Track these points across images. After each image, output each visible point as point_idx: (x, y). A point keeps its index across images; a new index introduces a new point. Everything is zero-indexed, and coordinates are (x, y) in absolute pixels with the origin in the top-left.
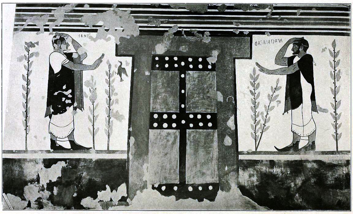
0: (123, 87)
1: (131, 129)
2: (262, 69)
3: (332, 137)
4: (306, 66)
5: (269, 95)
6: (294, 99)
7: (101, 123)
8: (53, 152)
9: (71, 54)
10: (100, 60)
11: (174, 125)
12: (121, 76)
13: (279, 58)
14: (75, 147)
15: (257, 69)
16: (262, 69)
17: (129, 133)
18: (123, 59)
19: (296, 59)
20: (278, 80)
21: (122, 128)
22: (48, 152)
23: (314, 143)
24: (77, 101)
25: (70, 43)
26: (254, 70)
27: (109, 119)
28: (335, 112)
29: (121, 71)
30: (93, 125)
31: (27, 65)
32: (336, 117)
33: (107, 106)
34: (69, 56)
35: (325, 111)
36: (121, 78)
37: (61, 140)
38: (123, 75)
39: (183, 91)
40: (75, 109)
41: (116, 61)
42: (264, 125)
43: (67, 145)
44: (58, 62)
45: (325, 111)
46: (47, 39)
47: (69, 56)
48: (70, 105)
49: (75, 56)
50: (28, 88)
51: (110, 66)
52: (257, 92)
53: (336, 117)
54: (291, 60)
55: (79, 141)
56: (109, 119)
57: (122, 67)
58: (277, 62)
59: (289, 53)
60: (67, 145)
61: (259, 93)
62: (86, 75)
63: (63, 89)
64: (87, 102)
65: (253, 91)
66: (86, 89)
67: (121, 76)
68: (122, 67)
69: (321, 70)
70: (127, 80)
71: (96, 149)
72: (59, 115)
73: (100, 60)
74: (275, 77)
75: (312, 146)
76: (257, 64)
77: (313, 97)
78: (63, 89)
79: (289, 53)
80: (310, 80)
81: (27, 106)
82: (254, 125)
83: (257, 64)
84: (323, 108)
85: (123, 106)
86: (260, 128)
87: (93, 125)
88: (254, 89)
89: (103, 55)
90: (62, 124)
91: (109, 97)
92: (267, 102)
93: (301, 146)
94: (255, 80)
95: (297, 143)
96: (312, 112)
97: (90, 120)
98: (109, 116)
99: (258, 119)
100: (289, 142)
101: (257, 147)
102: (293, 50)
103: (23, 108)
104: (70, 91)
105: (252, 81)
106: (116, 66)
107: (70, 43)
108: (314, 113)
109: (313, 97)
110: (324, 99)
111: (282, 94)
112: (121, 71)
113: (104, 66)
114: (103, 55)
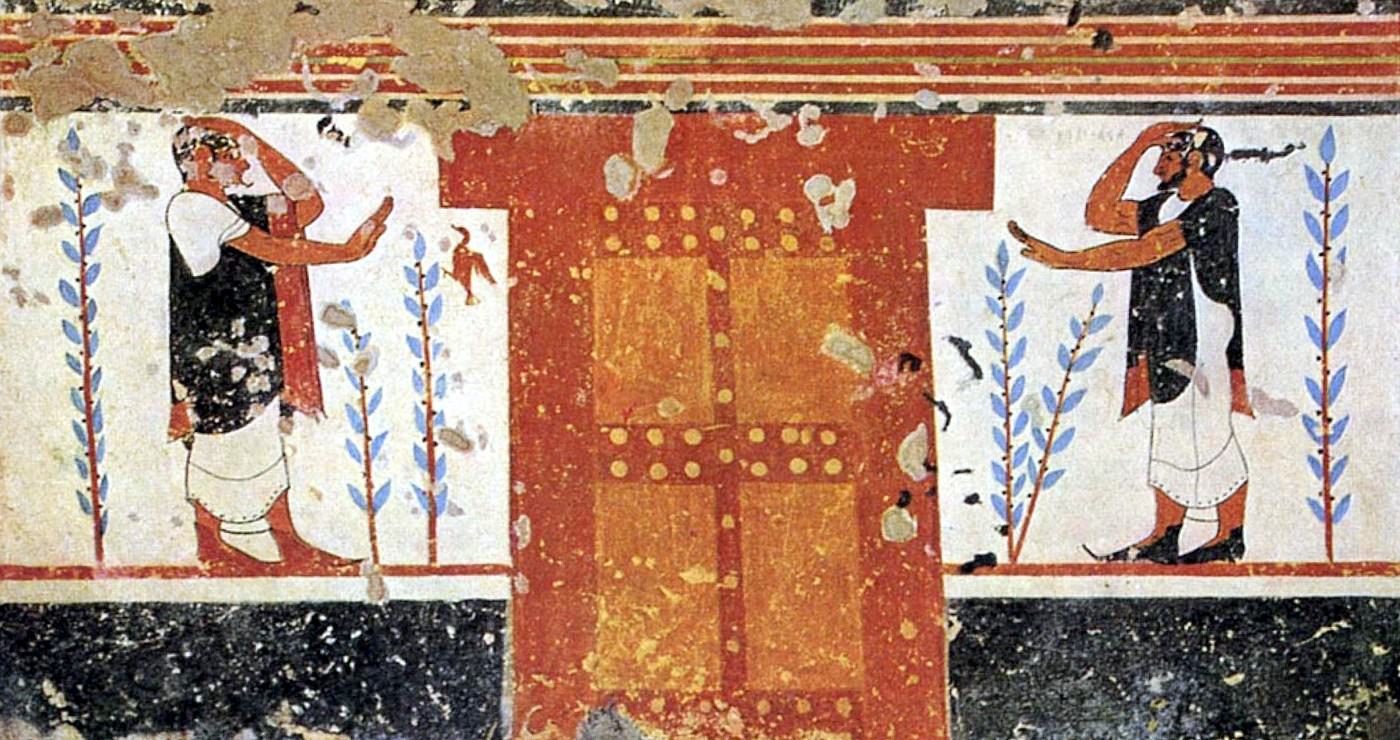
0: (479, 331)
1: (520, 488)
2: (1033, 247)
3: (1307, 510)
4: (1213, 236)
5: (1062, 348)
6: (1159, 354)
7: (398, 469)
8: (212, 574)
9: (260, 201)
10: (378, 221)
11: (692, 469)
12: (466, 283)
13: (1102, 205)
14: (298, 556)
15: (1015, 246)
16: (1033, 247)
17: (513, 499)
18: (470, 217)
19: (1171, 210)
20: (1098, 292)
21: (483, 482)
22: (188, 572)
23: (1237, 533)
24: (296, 380)
25: (252, 158)
26: (1002, 258)
27: (431, 452)
28: (1323, 412)
29: (466, 264)
30: (367, 474)
31: (75, 242)
32: (1326, 432)
33: (418, 437)
34: (251, 209)
35: (1285, 409)
36: (469, 292)
37: (236, 528)
38: (477, 279)
39: (728, 522)
40: (286, 410)
41: (439, 225)
42: (1051, 470)
43: (266, 548)
44: (206, 233)
45: (1285, 409)
46: (152, 148)
47: (251, 209)
48: (265, 398)
49: (276, 208)
50: (87, 332)
51: (420, 250)
52: (1013, 339)
53: (1326, 432)
54: (1148, 210)
55: (310, 529)
56: (431, 452)
57: (473, 246)
58: (1093, 216)
59: (1142, 184)
60: (266, 548)
61: (1022, 343)
62: (326, 283)
63: (236, 321)
64: (335, 386)
65: (1000, 333)
66: (326, 336)
67: (466, 283)
68: (473, 246)
69: (1270, 257)
70: (493, 297)
71: (382, 562)
72: (220, 439)
73: (378, 221)
74: (1089, 279)
75: (1227, 548)
76: (1014, 229)
77: (1234, 354)
78: (236, 321)
79: (1142, 184)
80: (1230, 297)
81: (89, 402)
82: (1003, 464)
83: (1014, 229)
84: (1275, 395)
85: (482, 401)
86: (1024, 480)
87: (367, 474)
88: (1004, 362)
89: (388, 204)
90: (243, 468)
91: (425, 364)
92: (1054, 377)
93: (1187, 543)
94: (1005, 287)
95: (1174, 531)
96: (1248, 558)
97: (354, 454)
98: (428, 438)
99: (1017, 442)
100: (1142, 525)
101: (1020, 545)
102: (1159, 171)
103: (79, 444)
104: (262, 342)
105: (997, 293)
106: (445, 245)
107: (252, 158)
108: (1240, 418)
109: (1234, 354)
110: (1280, 357)
111: (1113, 346)
112: (466, 264)
113: (392, 243)
114: (388, 204)
